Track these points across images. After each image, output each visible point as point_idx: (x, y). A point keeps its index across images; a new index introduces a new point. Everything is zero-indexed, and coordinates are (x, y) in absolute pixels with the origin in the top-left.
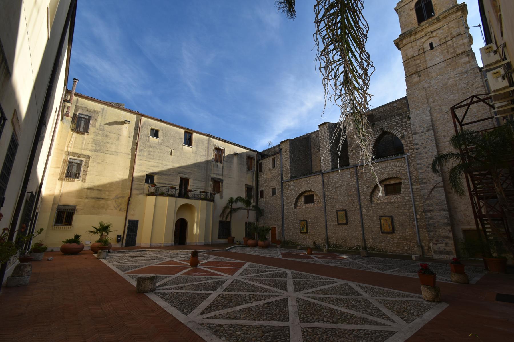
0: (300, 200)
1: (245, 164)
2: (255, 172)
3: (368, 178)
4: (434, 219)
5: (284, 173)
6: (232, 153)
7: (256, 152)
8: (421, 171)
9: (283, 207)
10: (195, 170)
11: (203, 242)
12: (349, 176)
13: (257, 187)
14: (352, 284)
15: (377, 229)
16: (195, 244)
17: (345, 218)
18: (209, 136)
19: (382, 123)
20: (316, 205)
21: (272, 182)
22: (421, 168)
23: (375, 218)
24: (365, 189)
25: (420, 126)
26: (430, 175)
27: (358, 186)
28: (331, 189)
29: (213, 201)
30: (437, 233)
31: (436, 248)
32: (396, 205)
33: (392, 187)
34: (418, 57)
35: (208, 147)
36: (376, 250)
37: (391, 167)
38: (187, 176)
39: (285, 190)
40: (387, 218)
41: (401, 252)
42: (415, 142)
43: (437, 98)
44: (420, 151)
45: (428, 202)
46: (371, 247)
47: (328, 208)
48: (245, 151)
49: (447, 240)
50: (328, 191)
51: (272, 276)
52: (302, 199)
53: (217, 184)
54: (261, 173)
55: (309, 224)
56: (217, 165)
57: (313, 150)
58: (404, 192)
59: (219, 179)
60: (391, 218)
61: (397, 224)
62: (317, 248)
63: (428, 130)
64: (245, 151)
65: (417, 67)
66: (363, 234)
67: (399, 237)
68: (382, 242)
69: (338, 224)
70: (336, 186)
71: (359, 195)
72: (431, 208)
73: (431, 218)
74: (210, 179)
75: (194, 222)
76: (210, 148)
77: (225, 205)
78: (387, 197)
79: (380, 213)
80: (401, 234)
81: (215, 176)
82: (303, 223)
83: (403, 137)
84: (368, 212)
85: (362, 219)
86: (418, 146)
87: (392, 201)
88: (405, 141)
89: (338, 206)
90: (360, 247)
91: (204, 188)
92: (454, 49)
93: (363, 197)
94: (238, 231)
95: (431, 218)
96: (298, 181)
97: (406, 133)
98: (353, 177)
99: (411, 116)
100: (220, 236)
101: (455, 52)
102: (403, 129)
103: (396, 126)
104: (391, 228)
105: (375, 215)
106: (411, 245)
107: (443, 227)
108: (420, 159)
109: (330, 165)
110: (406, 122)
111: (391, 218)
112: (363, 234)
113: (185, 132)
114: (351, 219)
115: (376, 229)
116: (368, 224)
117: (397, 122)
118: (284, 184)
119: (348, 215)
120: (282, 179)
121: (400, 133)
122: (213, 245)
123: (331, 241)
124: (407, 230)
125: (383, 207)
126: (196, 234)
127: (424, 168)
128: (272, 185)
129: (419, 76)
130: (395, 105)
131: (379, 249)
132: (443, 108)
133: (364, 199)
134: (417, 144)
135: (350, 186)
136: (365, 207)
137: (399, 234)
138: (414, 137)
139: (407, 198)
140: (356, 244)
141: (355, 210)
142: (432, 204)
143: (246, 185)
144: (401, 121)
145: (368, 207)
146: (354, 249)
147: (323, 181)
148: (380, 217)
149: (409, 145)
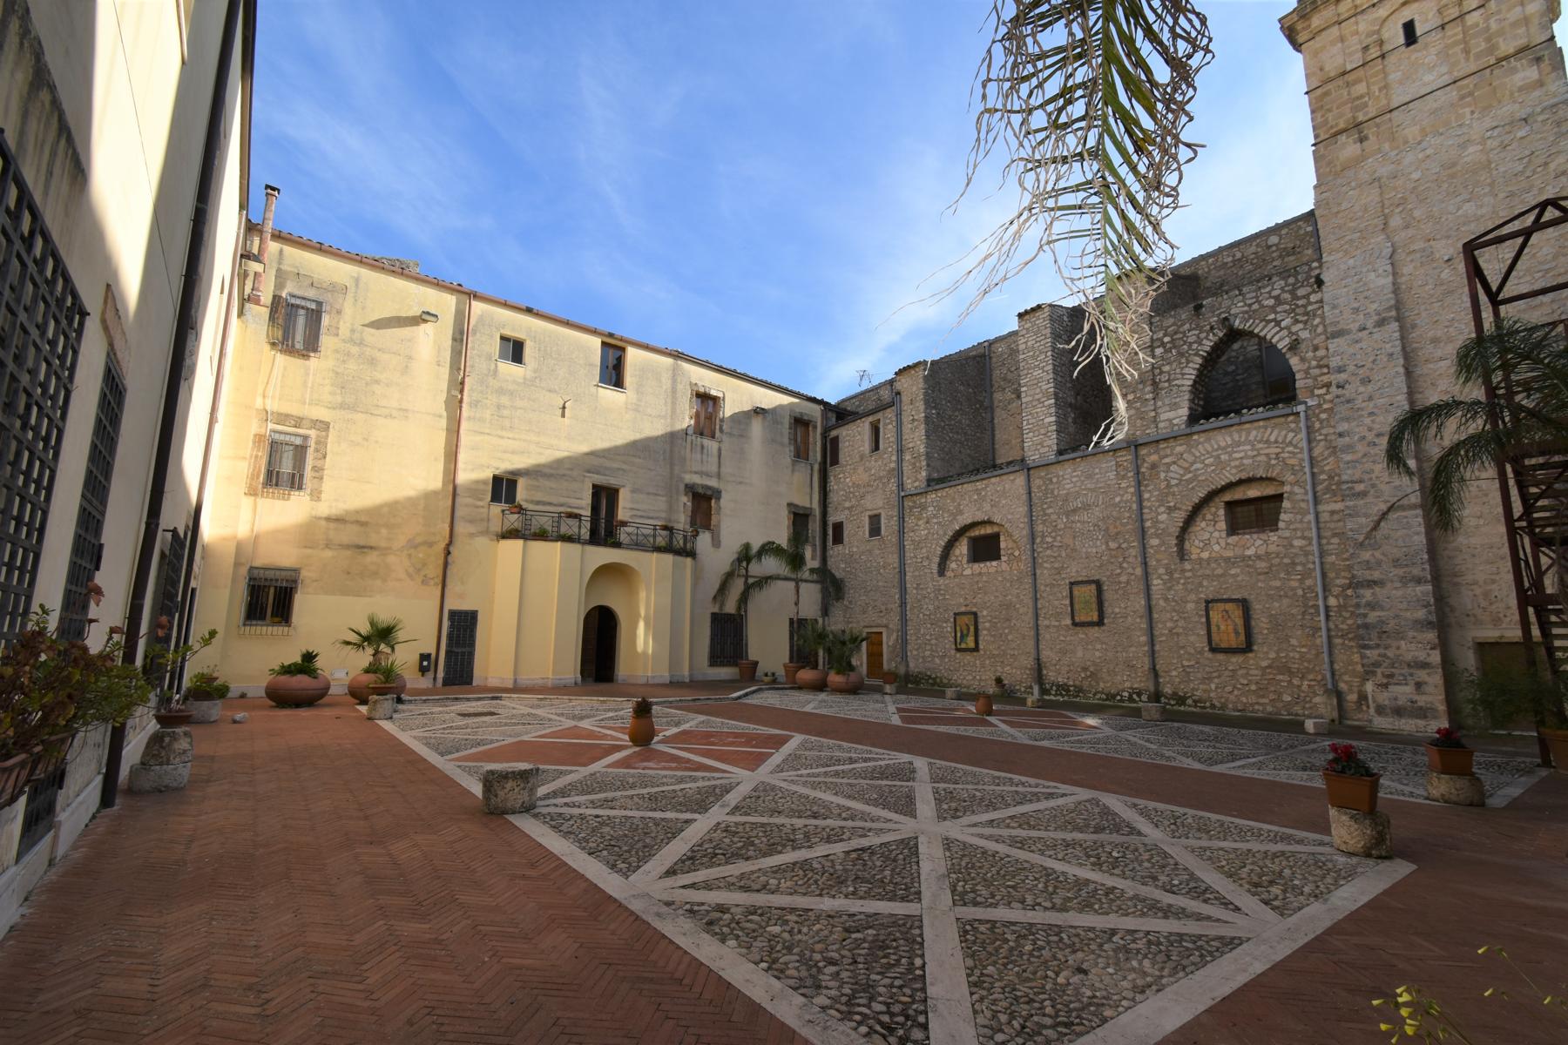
0: (957, 552)
2: (816, 467)
3: (1174, 482)
4: (1382, 609)
5: (907, 468)
6: (747, 408)
7: (821, 402)
8: (1348, 457)
11: (664, 675)
12: (1112, 475)
13: (824, 514)
14: (1114, 802)
15: (1198, 640)
16: (643, 681)
17: (1094, 606)
18: (678, 356)
20: (1004, 566)
22: (1349, 448)
23: (1190, 606)
24: (1163, 517)
25: (1356, 311)
27: (1141, 507)
28: (1054, 517)
29: (692, 554)
30: (1390, 653)
31: (1384, 698)
32: (1262, 565)
33: (1252, 510)
34: (1361, 72)
35: (674, 390)
36: (1189, 701)
37: (1243, 447)
39: (910, 521)
40: (1229, 606)
41: (1269, 709)
42: (1335, 362)
44: (1348, 392)
46: (1175, 694)
47: (1044, 574)
49: (1422, 675)
50: (1044, 522)
52: (962, 548)
53: (703, 502)
55: (984, 625)
57: (998, 396)
58: (1289, 523)
59: (709, 488)
61: (1261, 623)
65: (1356, 109)
67: (1264, 664)
68: (1210, 679)
69: (1075, 624)
70: (1071, 506)
72: (1376, 575)
73: (1372, 606)
74: (682, 487)
79: (1209, 589)
80: (1273, 655)
81: (697, 480)
82: (966, 619)
83: (1294, 346)
84: (1170, 589)
86: (1343, 376)
88: (1303, 360)
89: (1075, 571)
90: (1139, 694)
92: (1488, 40)
93: (1155, 542)
94: (768, 644)
95: (1372, 606)
96: (951, 491)
97: (1304, 335)
98: (1124, 477)
99: (1324, 277)
101: (1491, 49)
103: (1273, 309)
104: (1242, 637)
105: (1193, 597)
106: (1305, 687)
107: (1411, 634)
108: (1347, 419)
109: (1052, 441)
110: (1307, 297)
111: (1245, 605)
113: (603, 343)
114: (1113, 608)
115: (1192, 638)
116: (1169, 625)
118: (908, 503)
119: (1108, 595)
120: (901, 486)
121: (1285, 332)
122: (694, 684)
123: (1051, 675)
124: (1294, 642)
125: (1219, 571)
130: (1274, 240)
131: (1200, 701)
134: (1340, 370)
135: (1115, 505)
136: (1162, 571)
137: (1265, 653)
138: (1333, 345)
139: (1297, 543)
140: (1127, 684)
141: (1128, 583)
142: (1379, 563)
143: (789, 505)
144: (1292, 292)
148: (1208, 602)
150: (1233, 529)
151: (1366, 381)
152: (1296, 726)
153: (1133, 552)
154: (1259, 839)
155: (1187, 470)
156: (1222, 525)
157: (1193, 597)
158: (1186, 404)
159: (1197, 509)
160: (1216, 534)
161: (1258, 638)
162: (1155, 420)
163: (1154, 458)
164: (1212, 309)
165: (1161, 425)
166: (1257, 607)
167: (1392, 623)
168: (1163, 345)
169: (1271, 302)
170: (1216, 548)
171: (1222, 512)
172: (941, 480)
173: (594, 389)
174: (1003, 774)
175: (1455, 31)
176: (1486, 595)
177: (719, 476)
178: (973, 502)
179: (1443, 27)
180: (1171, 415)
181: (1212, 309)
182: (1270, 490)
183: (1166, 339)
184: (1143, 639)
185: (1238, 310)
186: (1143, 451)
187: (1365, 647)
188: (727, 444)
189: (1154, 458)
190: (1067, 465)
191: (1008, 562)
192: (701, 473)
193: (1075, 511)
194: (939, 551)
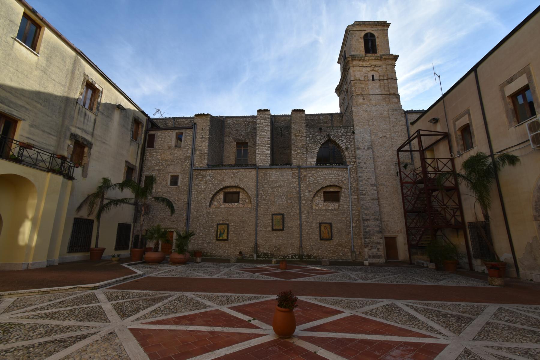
0: (218, 197)
1: (129, 128)
2: (141, 146)
3: (311, 183)
4: (370, 227)
5: (196, 158)
6: (113, 103)
7: (146, 115)
8: (361, 183)
9: (189, 204)
10: (39, 106)
11: (43, 261)
12: (290, 177)
13: (141, 170)
14: (400, 303)
15: (316, 236)
16: (24, 267)
17: (281, 223)
18: (79, 53)
19: (328, 130)
20: (241, 205)
21: (172, 167)
22: (361, 181)
23: (314, 224)
24: (307, 194)
25: (363, 143)
26: (368, 187)
27: (300, 189)
28: (267, 188)
29: (70, 177)
30: (372, 240)
31: (370, 253)
32: (336, 212)
33: (332, 195)
34: (363, 82)
35: (73, 73)
36: (312, 257)
37: (329, 176)
38: (15, 113)
39: (196, 181)
40: (327, 225)
41: (336, 258)
42: (358, 156)
43: (375, 123)
44: (361, 165)
45: (366, 212)
46: (307, 255)
47: (261, 210)
48: (132, 108)
49: (379, 246)
50: (262, 190)
51: (73, 302)
52: (221, 196)
53: (81, 146)
54: (152, 150)
55: (232, 229)
56: (85, 114)
57: (226, 138)
58: (343, 200)
59: (86, 140)
60: (330, 224)
61: (335, 230)
62: (241, 259)
63: (368, 149)
64: (132, 108)
65: (362, 91)
66: (301, 241)
67: (335, 244)
68: (319, 249)
69: (273, 230)
70: (274, 185)
71: (300, 199)
72: (368, 218)
73: (367, 226)
74: (68, 135)
75: (26, 217)
76: (76, 76)
77: (94, 190)
78: (325, 204)
79: (320, 219)
80: (337, 241)
81: (79, 133)
82: (223, 227)
83: (347, 148)
84: (308, 218)
85: (301, 225)
86: (360, 161)
87: (330, 208)
88: (348, 153)
89: (274, 210)
90: (295, 256)
91: (52, 149)
92: (388, 88)
93: (304, 202)
94: (105, 237)
95: (367, 226)
96: (220, 171)
97: (349, 146)
98: (295, 178)
99: (355, 132)
100: (73, 247)
101: (389, 91)
102: (347, 142)
103: (341, 136)
104: (330, 235)
105: (315, 221)
106: (346, 251)
107: (376, 234)
108: (361, 173)
109: (268, 160)
110: (350, 136)
111: (330, 224)
112: (301, 241)
113: (25, 14)
114: (288, 224)
115: (314, 235)
116: (307, 231)
117: (342, 133)
118: (195, 173)
119: (286, 219)
120: (192, 164)
121: (344, 144)
122: (63, 266)
123: (261, 250)
124: (343, 237)
125: (323, 213)
126: (28, 246)
127: (364, 181)
128: (171, 170)
129: (364, 99)
130: (321, 117)
131: (315, 257)
132: (379, 133)
133: (305, 203)
134: (359, 159)
135: (291, 187)
136: (305, 212)
137: (336, 241)
138: (357, 151)
139: (345, 206)
140: (291, 252)
141: (294, 215)
142: (369, 214)
143: (126, 162)
144: (346, 133)
145: (308, 213)
146: (289, 258)
147: (257, 178)
148: (320, 223)
149: (351, 157)
150: (225, 201)
151: (365, 163)
152: (362, 264)
153: (296, 205)
154: (448, 307)
155: (315, 179)
156: (322, 199)
157: (315, 221)
158: (316, 158)
159: (318, 192)
160: (321, 201)
161: (334, 236)
162: (306, 161)
163: (305, 173)
164: (325, 131)
165: (308, 163)
166: (334, 225)
167: (372, 231)
168: (309, 137)
169: (341, 134)
170: (320, 206)
171: (323, 194)
172: (214, 166)
173: (11, 40)
174: (221, 294)
175: (382, 82)
176: (387, 224)
177: (92, 135)
178: (229, 178)
179: (380, 80)
180: (311, 160)
181: (325, 131)
182: (336, 190)
183: (310, 136)
184: (298, 236)
185: (457, 129)
186: (302, 170)
187: (366, 238)
188: (100, 118)
189: (305, 173)
190: (273, 170)
191: (243, 204)
192: (82, 130)
193: (275, 187)
194: (211, 196)
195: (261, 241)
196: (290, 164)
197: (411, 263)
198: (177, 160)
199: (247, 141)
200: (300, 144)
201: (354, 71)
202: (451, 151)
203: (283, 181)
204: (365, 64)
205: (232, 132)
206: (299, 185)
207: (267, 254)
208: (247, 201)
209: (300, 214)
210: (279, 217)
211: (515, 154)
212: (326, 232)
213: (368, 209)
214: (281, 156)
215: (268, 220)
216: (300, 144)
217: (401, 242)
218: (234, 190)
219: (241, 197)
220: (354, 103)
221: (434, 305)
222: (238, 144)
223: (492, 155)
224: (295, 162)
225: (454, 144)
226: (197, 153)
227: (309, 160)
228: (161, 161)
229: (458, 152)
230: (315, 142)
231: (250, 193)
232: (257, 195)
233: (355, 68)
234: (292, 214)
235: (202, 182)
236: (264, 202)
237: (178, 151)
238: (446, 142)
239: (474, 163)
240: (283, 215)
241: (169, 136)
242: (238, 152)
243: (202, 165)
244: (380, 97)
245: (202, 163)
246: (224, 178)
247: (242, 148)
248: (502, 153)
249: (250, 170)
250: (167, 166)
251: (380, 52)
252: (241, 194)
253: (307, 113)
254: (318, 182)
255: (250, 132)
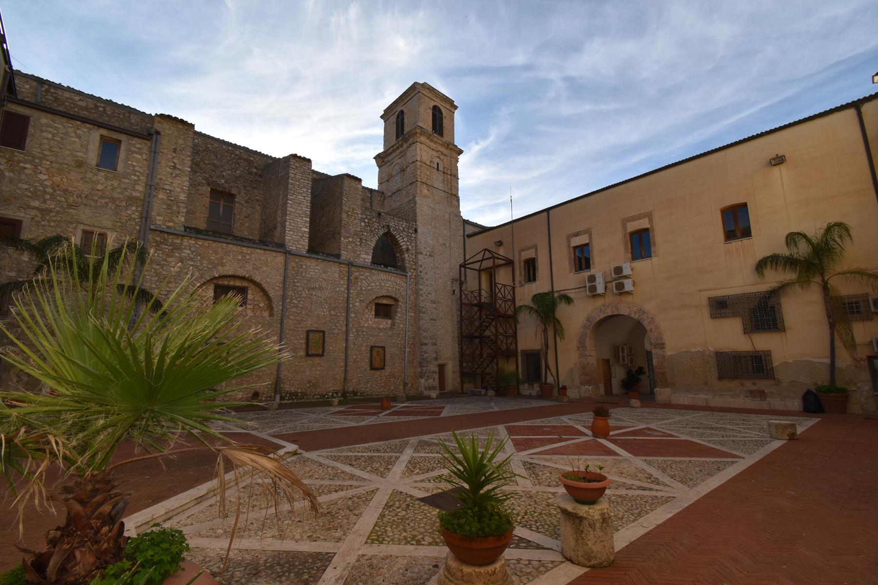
12: (337, 275)
17: (321, 345)
22: (422, 295)
23: (364, 348)
24: (357, 304)
28: (300, 289)
33: (384, 309)
37: (384, 283)
40: (380, 349)
42: (420, 263)
47: (289, 323)
50: (293, 290)
60: (383, 348)
63: (430, 256)
68: (368, 382)
70: (313, 285)
72: (426, 341)
73: (425, 352)
78: (376, 320)
79: (372, 341)
83: (408, 250)
87: (381, 326)
89: (310, 324)
90: (337, 393)
93: (353, 315)
95: (425, 352)
96: (214, 245)
98: (342, 279)
111: (383, 348)
114: (329, 347)
119: (327, 340)
120: (146, 217)
123: (287, 387)
141: (338, 334)
145: (357, 332)
156: (373, 313)
161: (387, 363)
162: (359, 256)
166: (387, 350)
178: (232, 260)
184: (342, 364)
186: (353, 269)
189: (357, 274)
190: (312, 261)
195: (287, 373)
196: (338, 256)
197: (462, 393)
198: (102, 197)
199: (234, 191)
200: (352, 230)
201: (421, 149)
202: (514, 280)
203: (325, 280)
204: (433, 145)
205: (202, 165)
206: (348, 289)
207: (295, 394)
208: (262, 305)
209: (347, 333)
210: (318, 336)
211: (571, 296)
212: (377, 359)
213: (426, 331)
214: (322, 242)
215: (301, 339)
216: (352, 230)
217: (452, 370)
218: (238, 283)
219: (250, 297)
220: (419, 192)
221: (346, 451)
222: (213, 191)
223: (552, 292)
224: (344, 255)
225: (517, 274)
226: (161, 196)
227: (363, 256)
228: (50, 190)
229: (520, 282)
230: (372, 231)
231: (272, 294)
232: (284, 297)
233: (423, 146)
234: (336, 331)
235: (170, 259)
236: (294, 310)
237: (107, 178)
238: (509, 269)
239: (539, 298)
240: (323, 332)
241: (79, 137)
242: (213, 208)
243: (171, 224)
244: (443, 194)
245: (171, 221)
246: (222, 258)
247: (222, 203)
248: (562, 293)
249: (274, 254)
250: (70, 206)
251: (446, 138)
252: (250, 292)
253: (364, 184)
254: (372, 289)
255: (241, 176)
